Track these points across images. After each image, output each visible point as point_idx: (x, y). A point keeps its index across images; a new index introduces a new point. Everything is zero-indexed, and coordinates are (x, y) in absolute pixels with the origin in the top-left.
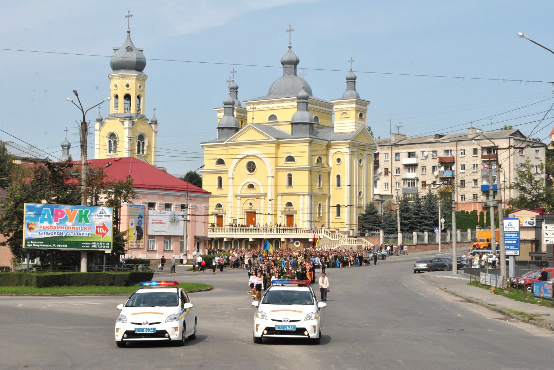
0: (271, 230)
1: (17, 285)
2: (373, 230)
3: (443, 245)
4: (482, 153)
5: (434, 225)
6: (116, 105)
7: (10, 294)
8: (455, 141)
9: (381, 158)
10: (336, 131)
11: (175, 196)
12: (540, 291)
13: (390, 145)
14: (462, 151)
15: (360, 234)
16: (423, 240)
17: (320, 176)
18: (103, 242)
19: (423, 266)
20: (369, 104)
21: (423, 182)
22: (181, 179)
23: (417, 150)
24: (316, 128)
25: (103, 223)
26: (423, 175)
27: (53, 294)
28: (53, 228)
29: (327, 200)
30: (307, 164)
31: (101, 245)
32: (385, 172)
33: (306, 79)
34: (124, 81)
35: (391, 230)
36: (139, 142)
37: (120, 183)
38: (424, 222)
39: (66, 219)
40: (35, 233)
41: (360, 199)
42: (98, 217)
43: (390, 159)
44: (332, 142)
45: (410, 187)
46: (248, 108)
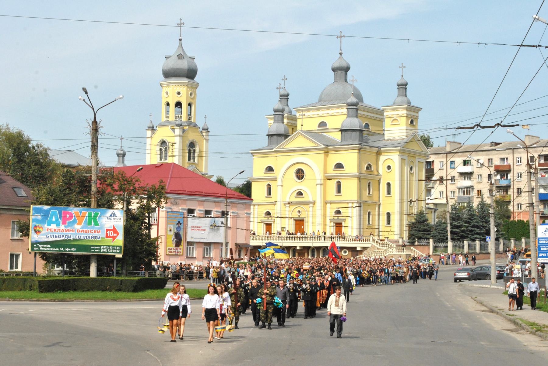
0: (319, 237)
1: (21, 290)
2: (423, 239)
3: (497, 254)
4: (539, 161)
6: (168, 113)
7: (7, 299)
8: (511, 149)
9: (436, 167)
13: (445, 153)
14: (518, 159)
15: (410, 242)
16: (475, 249)
17: (369, 183)
18: (113, 246)
19: (464, 275)
20: (421, 110)
21: (478, 191)
23: (474, 157)
24: (365, 135)
25: (114, 226)
26: (478, 184)
27: (51, 300)
28: (61, 231)
29: (377, 208)
30: (356, 172)
31: (111, 249)
33: (356, 84)
34: (175, 88)
35: (441, 239)
36: (190, 150)
37: (153, 188)
38: (475, 231)
39: (74, 222)
42: (108, 220)
43: (445, 167)
44: (382, 149)
45: (466, 195)
46: (298, 114)
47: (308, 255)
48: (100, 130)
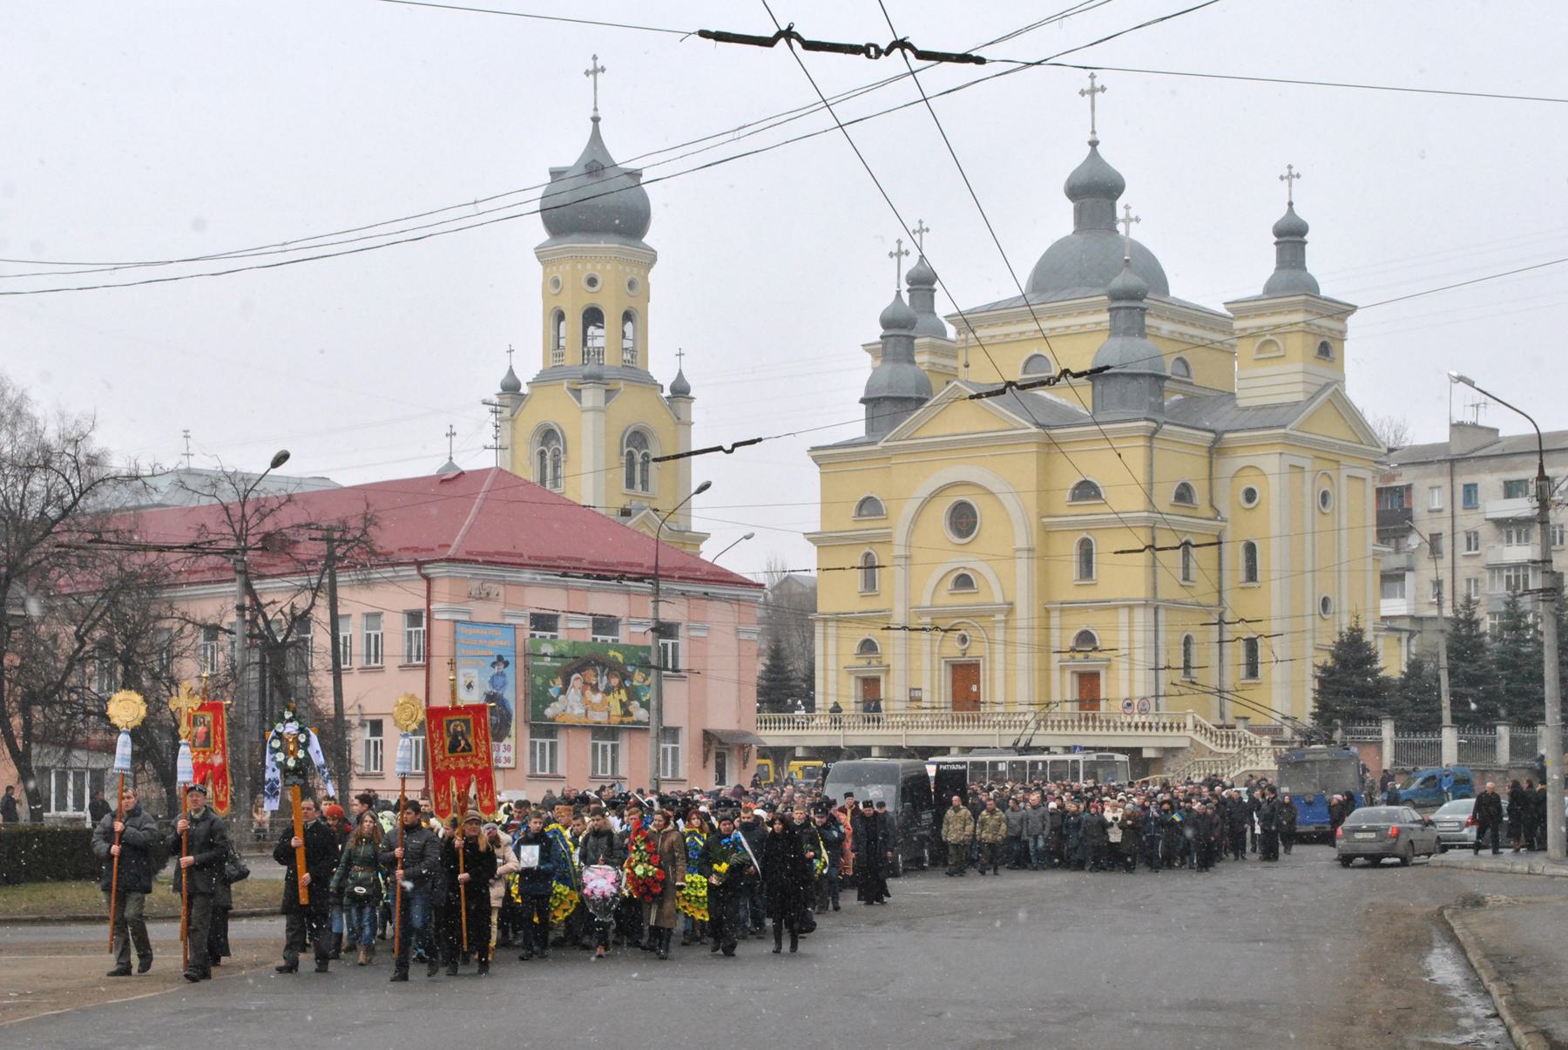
34: (579, 266)
44: (1227, 436)
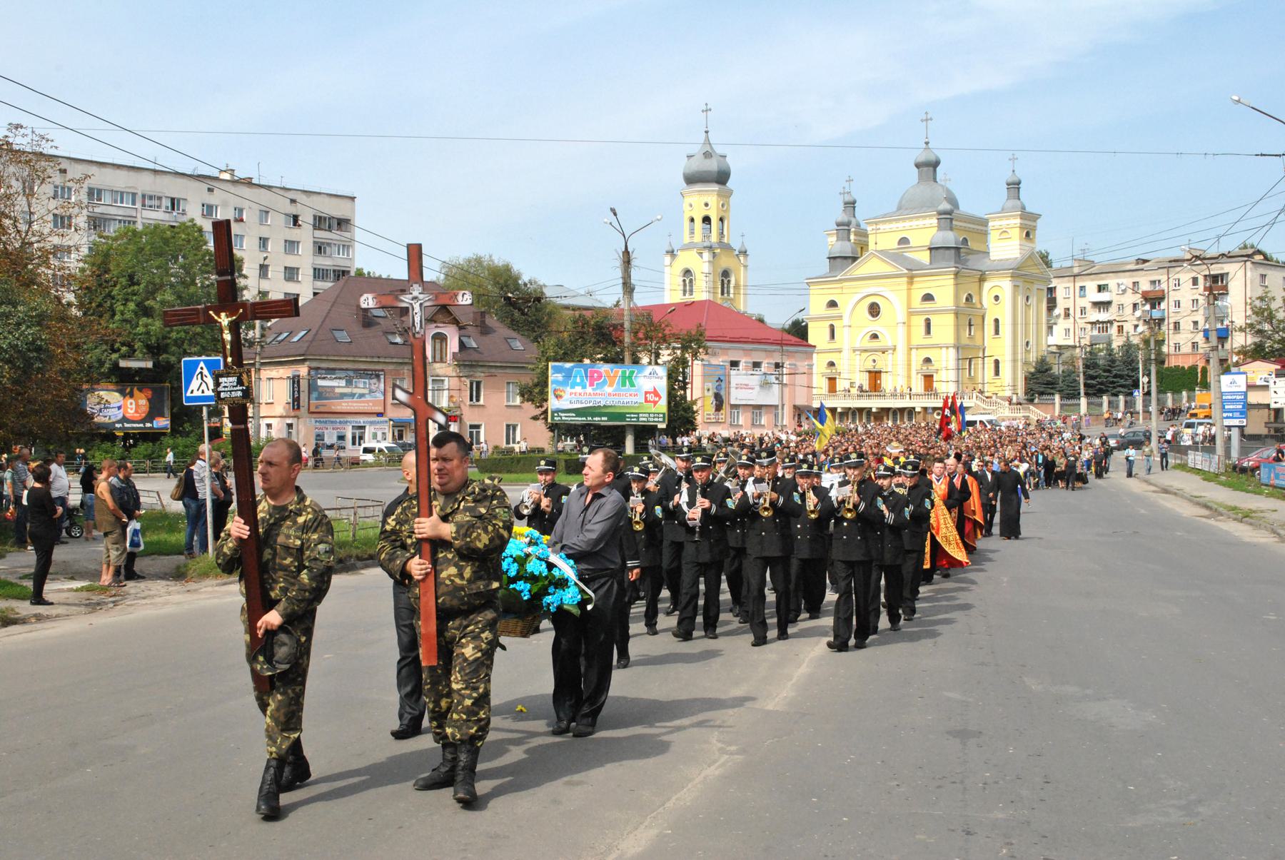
0: (902, 396)
5: (1132, 386)
6: (692, 232)
8: (1165, 267)
9: (1060, 295)
10: (992, 258)
11: (766, 351)
12: (1269, 478)
15: (1027, 400)
22: (784, 330)
23: (1112, 282)
32: (1065, 313)
33: (949, 186)
36: (723, 281)
39: (604, 383)
40: (564, 403)
41: (1027, 352)
46: (869, 229)
47: (888, 419)
48: (634, 263)
